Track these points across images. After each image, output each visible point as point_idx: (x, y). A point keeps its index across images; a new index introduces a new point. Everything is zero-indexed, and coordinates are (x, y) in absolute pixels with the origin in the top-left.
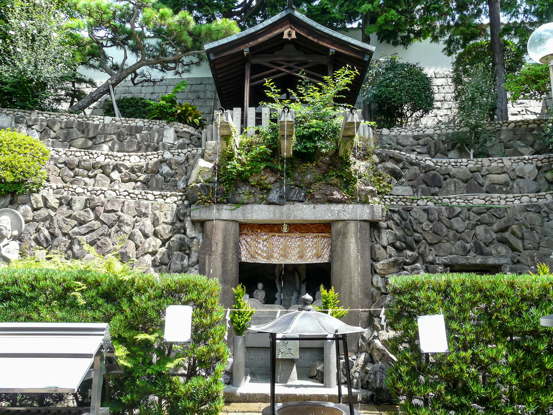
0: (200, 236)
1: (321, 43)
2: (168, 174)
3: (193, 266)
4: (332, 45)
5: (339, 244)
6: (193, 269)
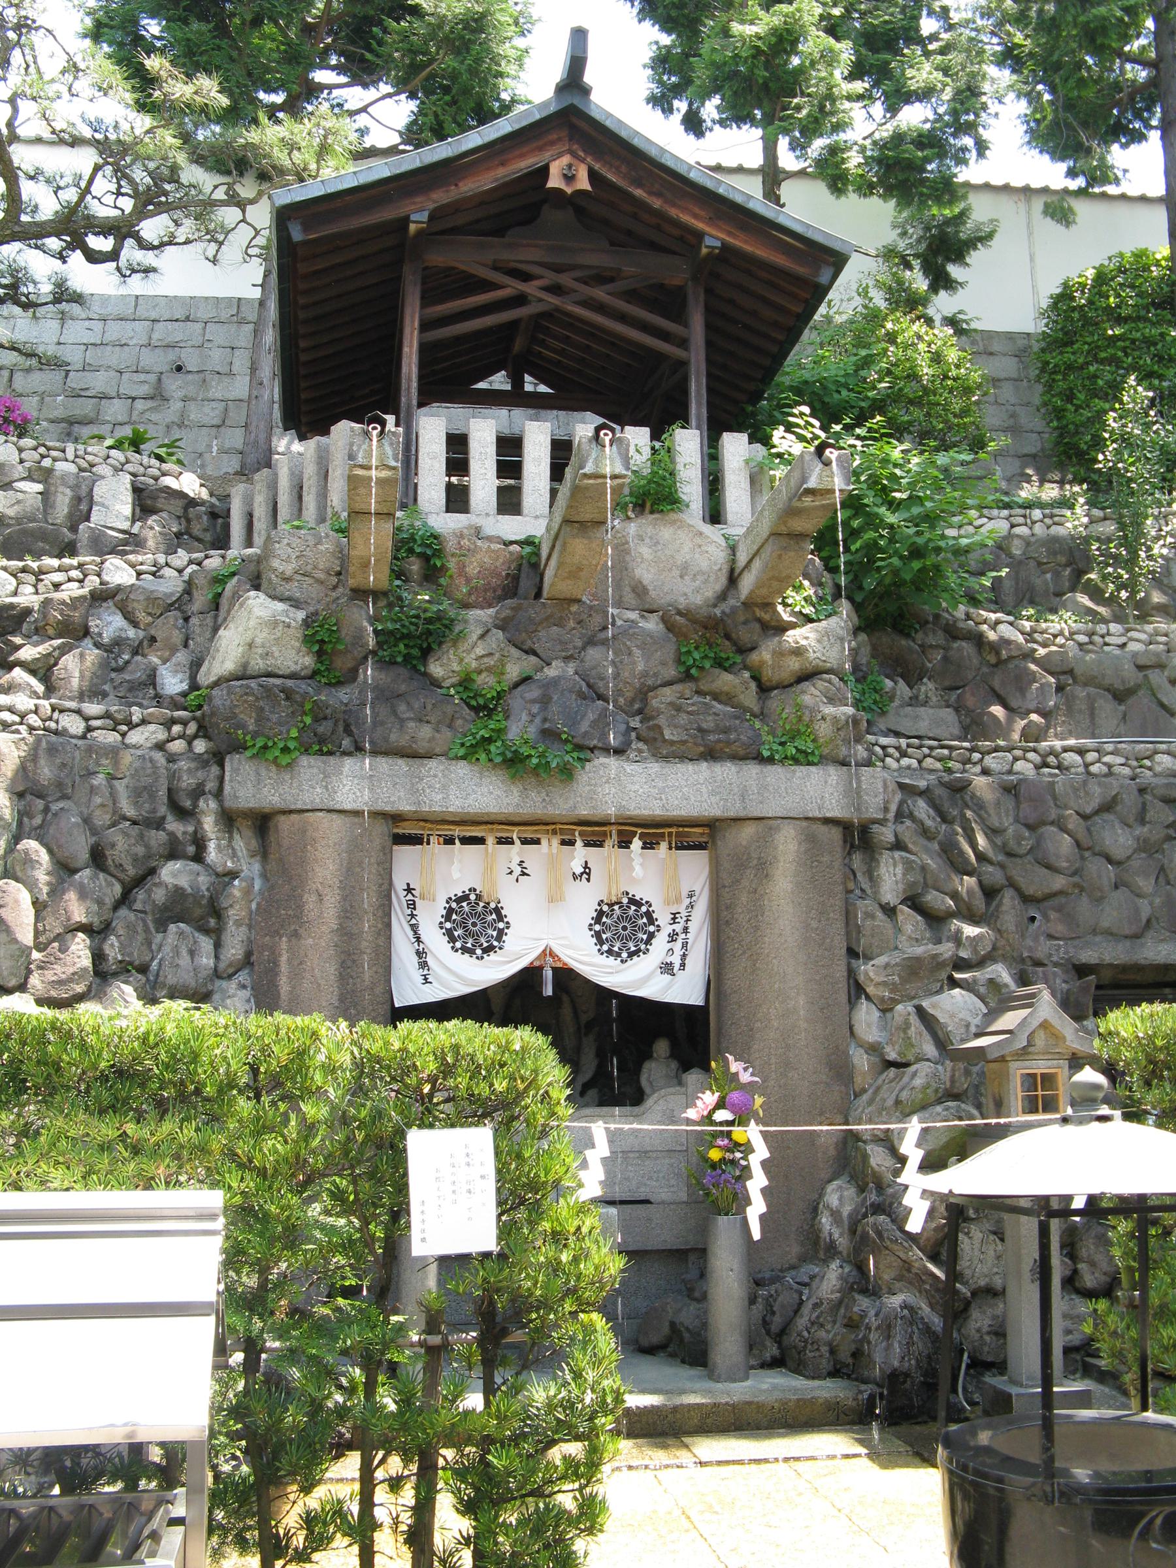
0: (251, 868)
1: (673, 212)
2: (118, 642)
3: (230, 977)
4: (710, 221)
5: (744, 899)
6: (232, 986)
